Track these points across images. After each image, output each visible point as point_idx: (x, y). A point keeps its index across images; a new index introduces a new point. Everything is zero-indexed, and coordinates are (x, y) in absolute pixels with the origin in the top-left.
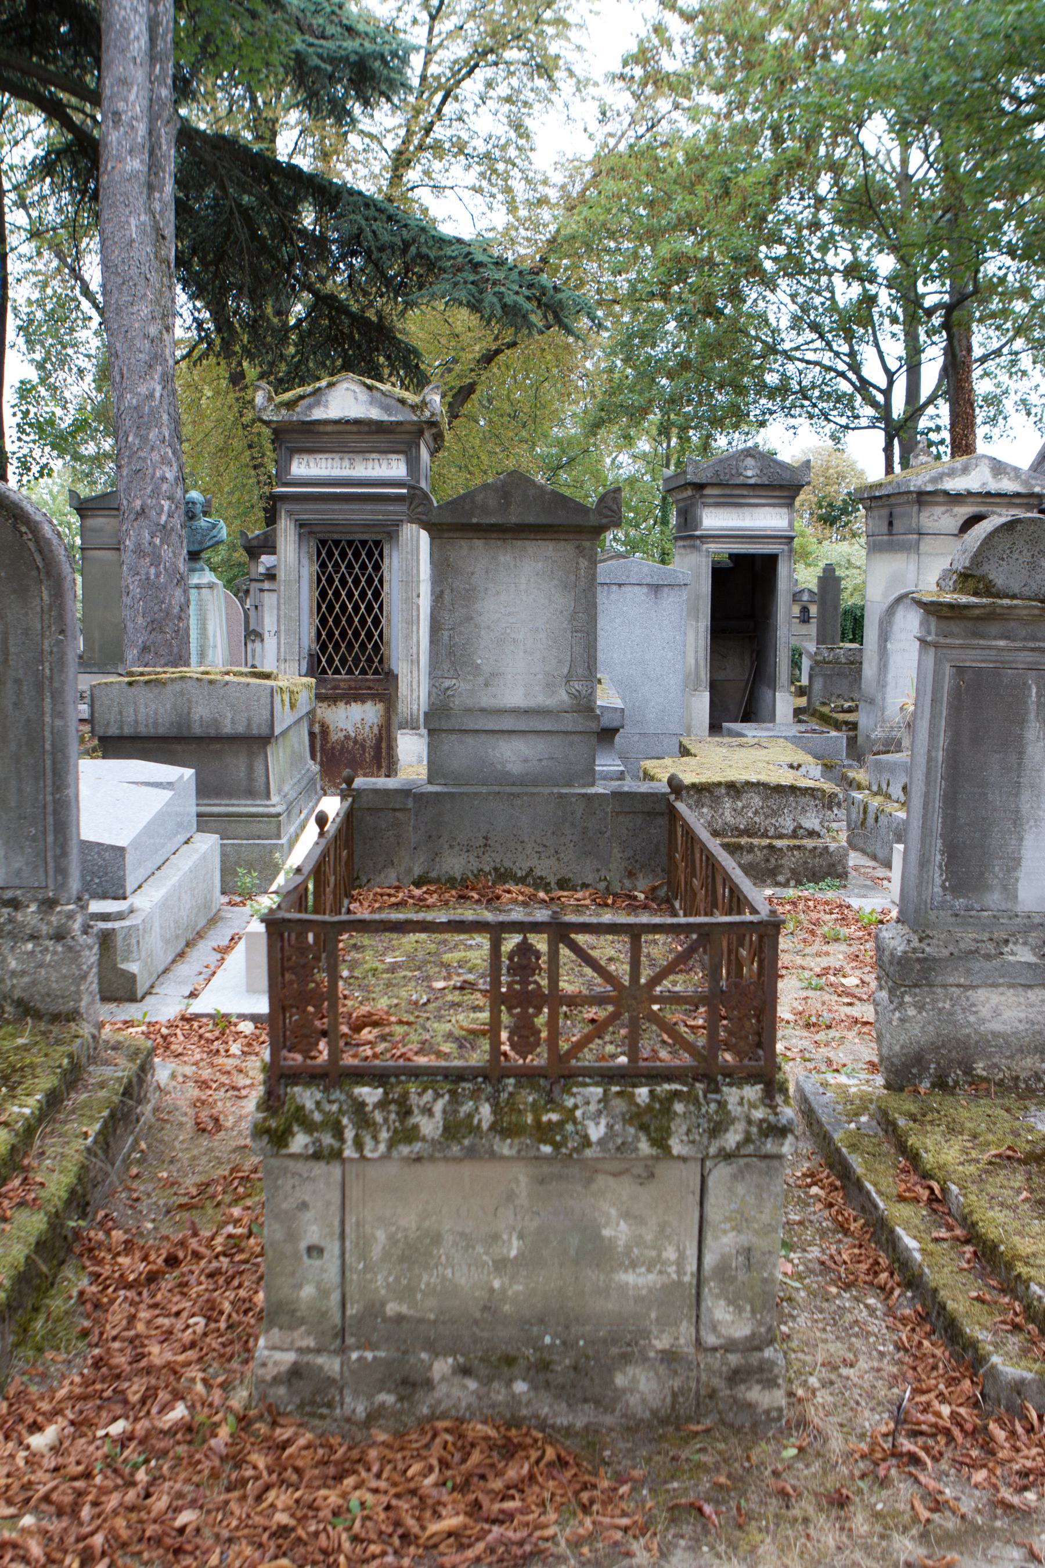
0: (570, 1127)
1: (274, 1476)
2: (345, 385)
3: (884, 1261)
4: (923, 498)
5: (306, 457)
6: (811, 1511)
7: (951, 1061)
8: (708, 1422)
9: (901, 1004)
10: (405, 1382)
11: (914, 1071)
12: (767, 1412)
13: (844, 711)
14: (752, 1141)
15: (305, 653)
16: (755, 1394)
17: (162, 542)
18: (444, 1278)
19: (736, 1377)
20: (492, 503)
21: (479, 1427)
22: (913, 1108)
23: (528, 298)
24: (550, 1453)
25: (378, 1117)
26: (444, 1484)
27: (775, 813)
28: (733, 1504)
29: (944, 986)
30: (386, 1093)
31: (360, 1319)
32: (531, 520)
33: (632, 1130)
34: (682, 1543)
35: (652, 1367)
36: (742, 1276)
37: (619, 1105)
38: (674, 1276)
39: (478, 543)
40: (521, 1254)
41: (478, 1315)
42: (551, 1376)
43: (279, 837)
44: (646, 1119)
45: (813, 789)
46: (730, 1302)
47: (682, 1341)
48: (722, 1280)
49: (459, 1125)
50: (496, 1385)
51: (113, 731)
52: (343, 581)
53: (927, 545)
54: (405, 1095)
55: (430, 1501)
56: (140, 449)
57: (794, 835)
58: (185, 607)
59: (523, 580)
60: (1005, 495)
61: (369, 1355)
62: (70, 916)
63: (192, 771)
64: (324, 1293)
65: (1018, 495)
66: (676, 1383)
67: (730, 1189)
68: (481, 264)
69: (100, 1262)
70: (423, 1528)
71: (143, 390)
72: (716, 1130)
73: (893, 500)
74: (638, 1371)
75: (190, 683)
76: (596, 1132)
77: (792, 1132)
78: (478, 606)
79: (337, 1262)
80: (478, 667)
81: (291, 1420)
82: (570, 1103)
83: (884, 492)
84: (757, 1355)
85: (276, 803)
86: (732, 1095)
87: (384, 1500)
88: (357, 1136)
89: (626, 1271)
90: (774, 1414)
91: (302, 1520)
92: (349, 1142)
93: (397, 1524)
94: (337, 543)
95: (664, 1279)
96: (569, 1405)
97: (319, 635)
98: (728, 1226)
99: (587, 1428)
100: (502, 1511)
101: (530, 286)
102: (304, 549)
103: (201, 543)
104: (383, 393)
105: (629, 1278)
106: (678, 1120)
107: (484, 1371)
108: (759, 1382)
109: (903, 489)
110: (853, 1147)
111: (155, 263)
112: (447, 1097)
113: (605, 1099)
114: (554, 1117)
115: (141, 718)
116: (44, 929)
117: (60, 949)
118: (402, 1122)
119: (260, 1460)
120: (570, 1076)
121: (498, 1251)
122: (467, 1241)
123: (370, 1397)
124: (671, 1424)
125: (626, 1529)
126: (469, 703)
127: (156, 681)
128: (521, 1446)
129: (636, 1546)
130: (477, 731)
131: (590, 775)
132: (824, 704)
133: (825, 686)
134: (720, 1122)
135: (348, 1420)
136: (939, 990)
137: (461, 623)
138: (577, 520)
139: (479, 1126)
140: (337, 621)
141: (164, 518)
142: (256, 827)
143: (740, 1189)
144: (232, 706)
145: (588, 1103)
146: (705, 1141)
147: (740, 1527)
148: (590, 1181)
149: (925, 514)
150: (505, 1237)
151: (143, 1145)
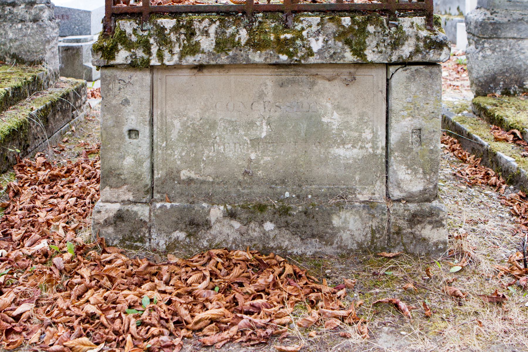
0: (299, 42)
1: (93, 283)
3: (491, 172)
6: (477, 307)
7: (512, 80)
8: (396, 252)
9: (483, 48)
10: (192, 223)
11: (492, 85)
12: (436, 244)
14: (421, 52)
16: (428, 232)
18: (218, 152)
19: (415, 219)
21: (241, 253)
22: (494, 102)
24: (289, 269)
25: (173, 37)
26: (213, 289)
28: (420, 303)
29: (505, 38)
30: (178, 21)
31: (163, 182)
33: (340, 44)
34: (386, 329)
35: (358, 212)
36: (416, 148)
37: (331, 27)
38: (371, 150)
40: (269, 136)
41: (241, 178)
42: (289, 219)
44: (349, 36)
46: (409, 167)
47: (377, 196)
48: (403, 151)
49: (226, 41)
50: (252, 225)
54: (191, 22)
55: (201, 299)
61: (168, 205)
62: (41, 10)
64: (139, 162)
66: (374, 224)
67: (406, 88)
69: (25, 173)
70: (193, 317)
72: (396, 45)
74: (348, 214)
76: (316, 45)
77: (446, 45)
79: (148, 140)
81: (116, 249)
82: (299, 27)
84: (428, 204)
86: (405, 22)
87: (168, 297)
88: (159, 50)
89: (338, 147)
90: (441, 246)
91: (105, 311)
92: (154, 55)
93: (175, 313)
95: (362, 153)
96: (302, 239)
98: (405, 113)
99: (314, 256)
100: (252, 306)
105: (340, 151)
106: (370, 38)
107: (244, 216)
108: (430, 223)
110: (463, 122)
112: (218, 23)
113: (321, 24)
114: (289, 36)
116: (28, 16)
117: (35, 26)
118: (188, 41)
119: (86, 272)
120: (299, 11)
121: (254, 133)
122: (233, 126)
123: (168, 234)
124: (372, 252)
125: (343, 319)
128: (269, 266)
129: (350, 331)
134: (398, 39)
135: (154, 250)
136: (503, 41)
139: (239, 43)
143: (413, 87)
145: (310, 26)
146: (389, 51)
147: (427, 317)
148: (313, 84)
150: (258, 124)
151: (74, 128)
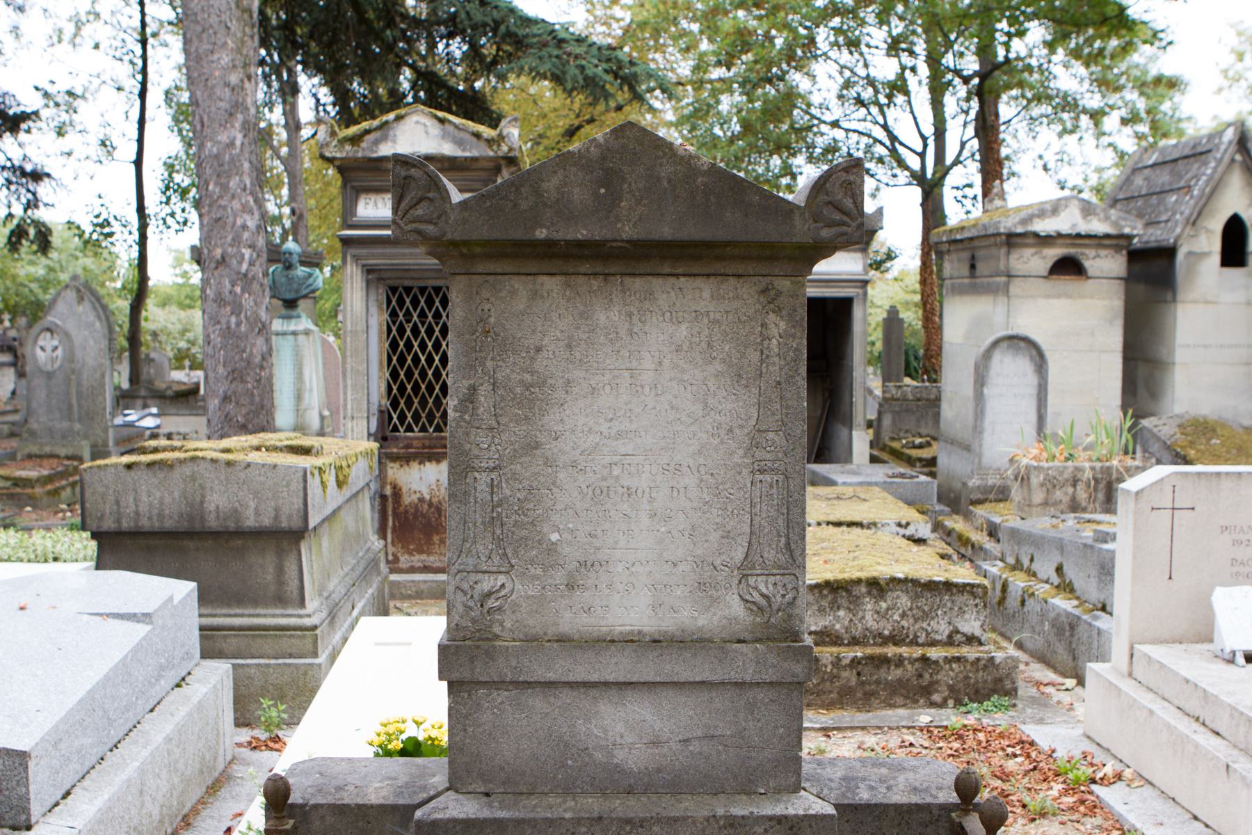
2: (415, 118)
4: (1012, 240)
5: (373, 197)
13: (915, 447)
15: (374, 409)
17: (243, 290)
20: (579, 195)
23: (606, 71)
27: (926, 616)
32: (666, 232)
39: (550, 284)
43: (315, 654)
45: (972, 586)
51: (109, 525)
52: (415, 331)
53: (1016, 287)
56: (221, 197)
57: (950, 642)
58: (268, 355)
59: (648, 363)
60: (1095, 237)
63: (194, 584)
65: (1107, 236)
68: (562, 41)
71: (223, 138)
73: (976, 243)
75: (203, 465)
78: (551, 419)
80: (552, 549)
83: (966, 235)
85: (314, 610)
94: (408, 290)
97: (390, 389)
101: (609, 60)
102: (373, 296)
103: (297, 291)
104: (456, 127)
109: (991, 231)
111: (238, 13)
115: (143, 508)
126: (535, 624)
127: (161, 464)
130: (551, 684)
131: (788, 770)
132: (893, 439)
133: (894, 423)
137: (514, 457)
138: (768, 231)
140: (409, 375)
141: (245, 267)
142: (286, 643)
144: (256, 494)
149: (1014, 255)
